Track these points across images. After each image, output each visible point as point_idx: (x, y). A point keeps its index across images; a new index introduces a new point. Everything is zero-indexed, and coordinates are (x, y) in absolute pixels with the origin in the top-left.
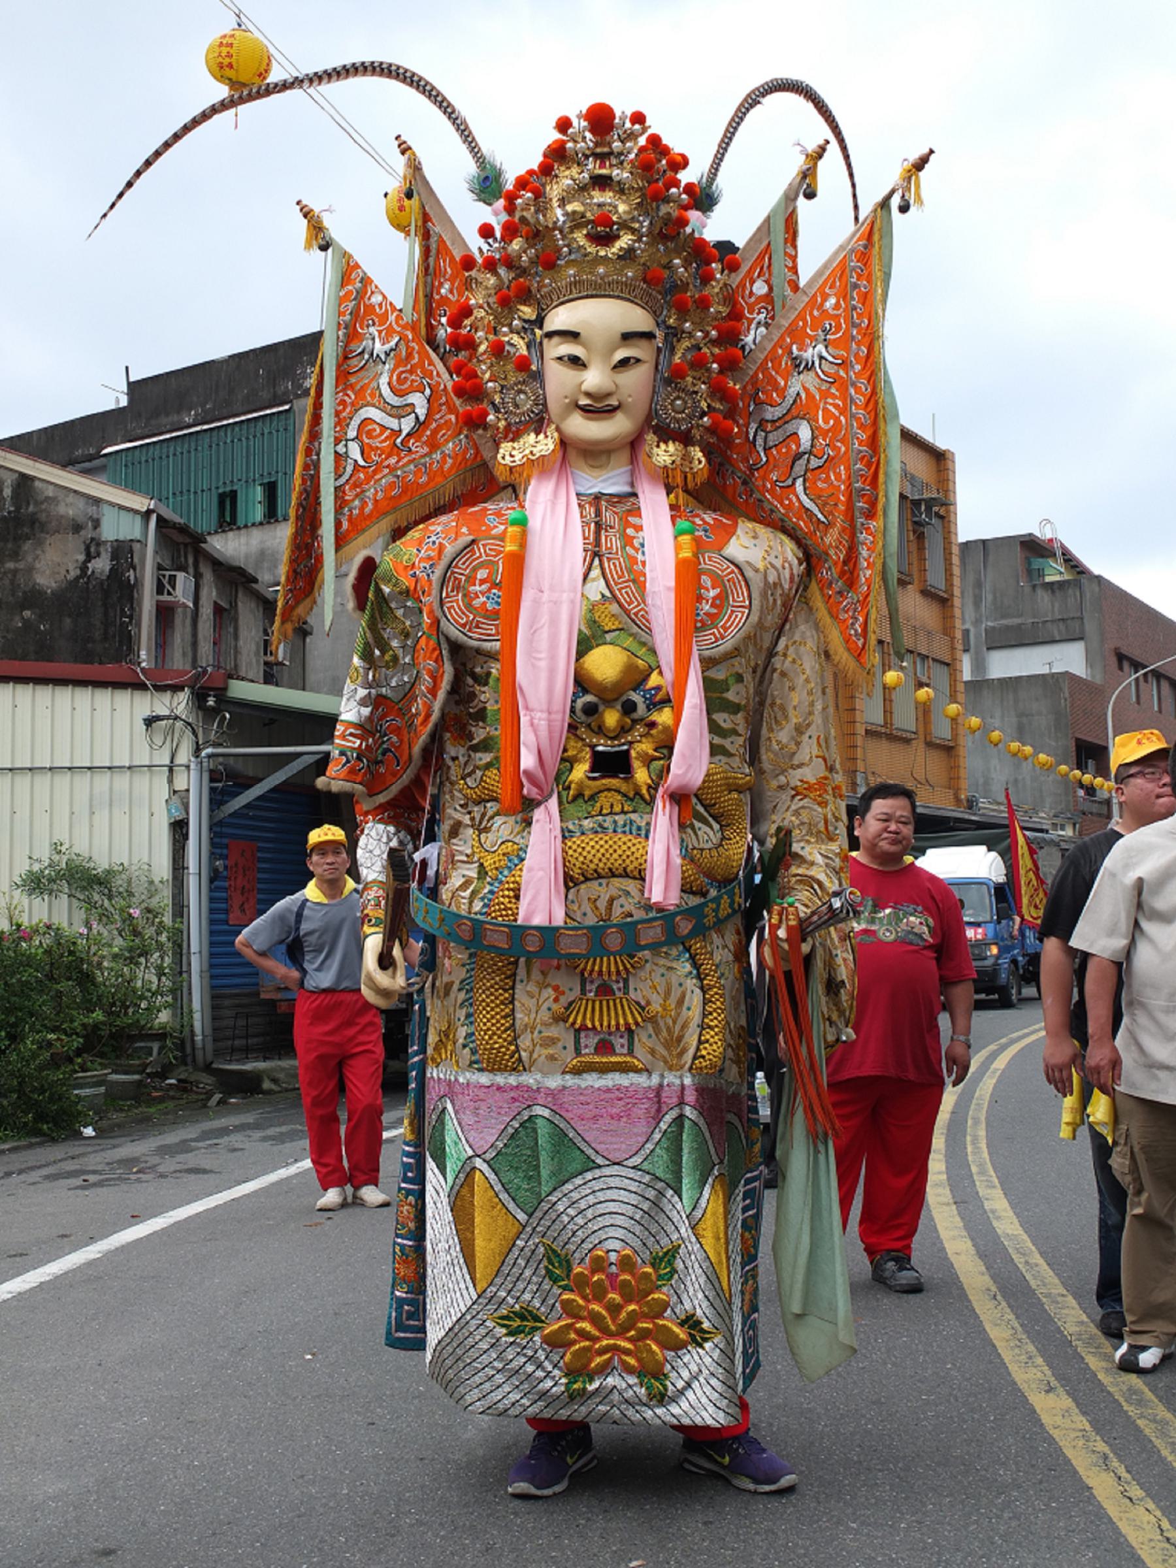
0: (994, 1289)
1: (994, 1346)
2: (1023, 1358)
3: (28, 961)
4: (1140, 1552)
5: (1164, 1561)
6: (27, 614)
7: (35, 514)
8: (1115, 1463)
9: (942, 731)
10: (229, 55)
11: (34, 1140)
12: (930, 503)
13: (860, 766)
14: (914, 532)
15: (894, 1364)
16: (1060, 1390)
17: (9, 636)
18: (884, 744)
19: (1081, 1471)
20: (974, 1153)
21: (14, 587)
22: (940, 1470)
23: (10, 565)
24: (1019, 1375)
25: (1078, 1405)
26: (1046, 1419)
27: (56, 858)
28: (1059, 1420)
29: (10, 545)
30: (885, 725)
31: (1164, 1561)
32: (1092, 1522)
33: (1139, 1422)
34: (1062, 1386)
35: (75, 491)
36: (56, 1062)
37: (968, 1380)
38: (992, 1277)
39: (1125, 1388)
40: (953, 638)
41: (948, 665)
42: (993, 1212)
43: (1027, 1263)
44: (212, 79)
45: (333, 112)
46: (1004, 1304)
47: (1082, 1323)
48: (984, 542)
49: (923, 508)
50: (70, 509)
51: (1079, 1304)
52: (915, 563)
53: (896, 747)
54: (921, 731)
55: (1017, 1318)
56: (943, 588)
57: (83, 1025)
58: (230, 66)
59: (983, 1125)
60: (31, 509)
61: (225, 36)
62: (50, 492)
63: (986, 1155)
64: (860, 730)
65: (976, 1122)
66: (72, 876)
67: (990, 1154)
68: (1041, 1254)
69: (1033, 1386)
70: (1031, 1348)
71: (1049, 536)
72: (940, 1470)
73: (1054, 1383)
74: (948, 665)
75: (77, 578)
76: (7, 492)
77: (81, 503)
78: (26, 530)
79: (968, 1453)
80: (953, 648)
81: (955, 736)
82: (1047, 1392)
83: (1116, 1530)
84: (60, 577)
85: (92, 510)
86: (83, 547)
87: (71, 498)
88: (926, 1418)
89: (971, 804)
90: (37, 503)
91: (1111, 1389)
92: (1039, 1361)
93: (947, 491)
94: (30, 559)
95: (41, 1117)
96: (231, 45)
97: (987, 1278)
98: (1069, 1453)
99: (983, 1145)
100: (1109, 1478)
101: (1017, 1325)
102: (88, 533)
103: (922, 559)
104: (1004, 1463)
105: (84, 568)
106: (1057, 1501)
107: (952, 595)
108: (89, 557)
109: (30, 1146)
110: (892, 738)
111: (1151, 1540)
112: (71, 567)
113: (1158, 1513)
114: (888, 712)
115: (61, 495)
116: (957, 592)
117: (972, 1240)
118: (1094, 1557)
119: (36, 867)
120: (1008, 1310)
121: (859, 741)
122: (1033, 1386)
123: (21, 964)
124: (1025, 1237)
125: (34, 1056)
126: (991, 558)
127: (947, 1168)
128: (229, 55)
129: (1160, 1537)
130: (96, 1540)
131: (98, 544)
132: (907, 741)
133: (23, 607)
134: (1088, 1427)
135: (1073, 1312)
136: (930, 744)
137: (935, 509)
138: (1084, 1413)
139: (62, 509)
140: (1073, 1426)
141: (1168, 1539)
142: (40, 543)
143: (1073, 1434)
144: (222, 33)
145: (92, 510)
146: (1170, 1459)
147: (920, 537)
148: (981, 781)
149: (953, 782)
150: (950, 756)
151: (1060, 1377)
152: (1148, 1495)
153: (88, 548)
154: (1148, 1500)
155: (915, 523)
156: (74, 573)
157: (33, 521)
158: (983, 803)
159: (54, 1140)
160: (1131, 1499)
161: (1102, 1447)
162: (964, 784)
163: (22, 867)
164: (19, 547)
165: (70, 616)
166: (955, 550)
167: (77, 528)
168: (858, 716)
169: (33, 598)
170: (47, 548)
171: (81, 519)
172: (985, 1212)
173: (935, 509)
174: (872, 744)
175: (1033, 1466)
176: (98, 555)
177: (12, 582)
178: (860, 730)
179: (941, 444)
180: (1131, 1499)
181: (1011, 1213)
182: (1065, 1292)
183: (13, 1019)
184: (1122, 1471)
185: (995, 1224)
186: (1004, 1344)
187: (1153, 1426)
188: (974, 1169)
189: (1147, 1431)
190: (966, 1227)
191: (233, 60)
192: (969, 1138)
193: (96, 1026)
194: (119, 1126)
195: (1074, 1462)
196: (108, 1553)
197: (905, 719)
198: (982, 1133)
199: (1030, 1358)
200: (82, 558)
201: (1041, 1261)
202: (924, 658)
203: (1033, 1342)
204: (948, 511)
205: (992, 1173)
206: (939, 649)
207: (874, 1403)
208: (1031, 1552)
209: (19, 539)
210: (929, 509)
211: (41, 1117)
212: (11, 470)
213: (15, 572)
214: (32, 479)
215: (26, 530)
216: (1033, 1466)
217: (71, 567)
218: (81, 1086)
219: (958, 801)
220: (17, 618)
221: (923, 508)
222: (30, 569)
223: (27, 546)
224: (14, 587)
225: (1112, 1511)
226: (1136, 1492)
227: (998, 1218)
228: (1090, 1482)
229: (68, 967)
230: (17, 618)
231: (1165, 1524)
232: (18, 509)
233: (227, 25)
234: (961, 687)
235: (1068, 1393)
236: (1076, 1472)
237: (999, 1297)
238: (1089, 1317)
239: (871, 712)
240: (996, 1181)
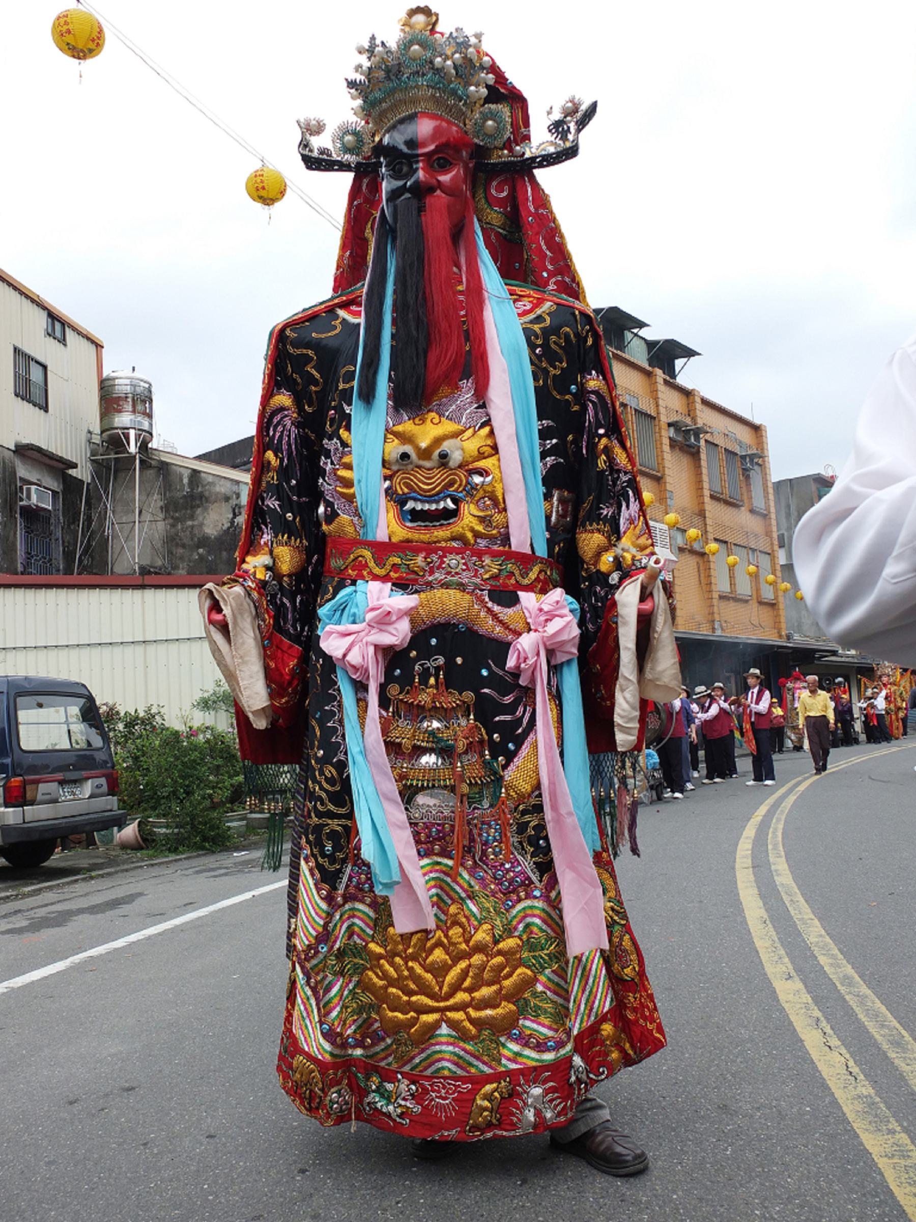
0: (766, 916)
1: (757, 952)
2: (776, 958)
3: (195, 747)
4: (828, 1082)
5: (845, 1087)
6: (201, 551)
7: (202, 492)
8: (824, 1023)
9: (768, 594)
10: (262, 182)
11: (200, 853)
12: (752, 457)
13: (717, 617)
14: (743, 475)
15: (687, 965)
16: (797, 979)
17: (191, 564)
18: (732, 604)
19: (798, 1029)
20: (773, 838)
21: (192, 536)
22: (699, 1031)
23: (190, 523)
24: (769, 969)
25: (806, 987)
26: (782, 997)
27: (217, 689)
28: (791, 997)
29: (189, 511)
30: (731, 593)
31: (845, 1087)
32: (799, 1063)
33: (847, 997)
34: (798, 975)
35: (225, 478)
36: (214, 807)
37: (734, 973)
38: (766, 910)
39: (841, 975)
40: (771, 538)
41: (769, 554)
42: (776, 871)
43: (792, 900)
44: (248, 197)
45: (303, 195)
46: (770, 926)
47: (821, 936)
48: (790, 480)
49: (748, 460)
50: (222, 488)
51: (821, 924)
52: (745, 494)
53: (739, 605)
54: (754, 593)
55: (777, 934)
56: (764, 507)
57: (231, 785)
58: (263, 188)
59: (782, 822)
60: (200, 489)
61: (257, 171)
62: (210, 479)
63: (780, 839)
64: (715, 595)
65: (778, 820)
66: (226, 699)
67: (783, 838)
68: (802, 894)
69: (778, 976)
70: (782, 952)
71: (831, 474)
72: (699, 1031)
73: (793, 973)
74: (769, 554)
75: (229, 528)
76: (186, 481)
77: (228, 484)
78: (198, 502)
79: (722, 1020)
80: (772, 544)
81: (776, 598)
82: (786, 979)
83: (815, 1069)
84: (219, 528)
85: (235, 488)
86: (231, 510)
87: (222, 482)
88: (699, 999)
89: (789, 637)
90: (203, 486)
91: (831, 976)
92: (786, 960)
93: (762, 449)
94: (201, 518)
95: (205, 839)
96: (262, 175)
97: (763, 911)
98: (792, 1018)
99: (780, 834)
100: (817, 1034)
101: (776, 939)
102: (234, 502)
103: (749, 491)
104: (745, 1027)
105: (232, 522)
106: (777, 1049)
107: (769, 512)
108: (235, 516)
109: (198, 856)
110: (736, 600)
111: (838, 1074)
112: (225, 522)
113: (848, 1056)
114: (732, 584)
115: (216, 480)
116: (773, 510)
117: (758, 888)
118: (795, 1087)
119: (206, 695)
120: (772, 929)
121: (715, 602)
122: (778, 976)
123: (191, 750)
124: (794, 885)
125: (200, 803)
126: (795, 489)
127: (753, 847)
128: (262, 182)
129: (845, 1072)
130: (126, 1082)
131: (240, 508)
132: (747, 601)
133: (198, 547)
134: (810, 1000)
135: (816, 929)
136: (761, 603)
137: (756, 460)
138: (809, 992)
139: (217, 489)
140: (800, 1000)
141: (851, 1073)
142: (206, 509)
143: (798, 1006)
144: (255, 169)
145: (235, 488)
146: (863, 1020)
147: (747, 478)
148: (796, 624)
149: (777, 625)
150: (774, 609)
151: (799, 970)
152: (843, 1044)
153: (234, 510)
154: (842, 1047)
155: (743, 469)
156: (227, 525)
157: (201, 496)
158: (796, 637)
159: (213, 852)
160: (830, 1047)
161: (817, 1013)
162: (783, 626)
163: (198, 695)
164: (194, 512)
165: (226, 550)
166: (770, 485)
167: (227, 499)
168: (713, 587)
169: (204, 541)
170: (210, 512)
171: (229, 494)
172: (771, 871)
173: (756, 460)
174: (723, 604)
175: (766, 1027)
176: (240, 514)
177: (191, 532)
178: (715, 595)
179: (757, 422)
180: (830, 1047)
181: (788, 872)
182: (813, 917)
183: (187, 783)
184: (829, 1030)
185: (776, 878)
186: (764, 950)
187: (856, 999)
188: (770, 847)
189: (851, 1003)
190: (756, 881)
191: (265, 184)
192: (771, 830)
193: (240, 785)
194: (255, 843)
195: (795, 1024)
196: (131, 1089)
197: (744, 587)
198: (781, 826)
199: (780, 958)
200: (231, 516)
201: (802, 900)
202: (754, 550)
203: (784, 948)
204: (764, 461)
205: (781, 848)
206: (762, 544)
207: (666, 989)
208: (750, 1084)
209: (193, 508)
210: (752, 461)
211: (205, 839)
212: (187, 468)
213: (192, 527)
214: (199, 472)
215: (198, 502)
216: (766, 1027)
217: (225, 522)
218: (232, 821)
219: (780, 636)
220: (195, 554)
221: (748, 460)
222: (201, 525)
223: (199, 511)
224: (192, 536)
225: (814, 1055)
226: (835, 1042)
227: (778, 875)
228: (803, 1037)
229: (221, 751)
230: (195, 554)
231: (851, 1063)
232: (192, 490)
233: (258, 165)
234: (778, 567)
235: (801, 979)
236: (795, 1030)
237: (768, 922)
238: (826, 931)
239: (722, 584)
240: (783, 853)
